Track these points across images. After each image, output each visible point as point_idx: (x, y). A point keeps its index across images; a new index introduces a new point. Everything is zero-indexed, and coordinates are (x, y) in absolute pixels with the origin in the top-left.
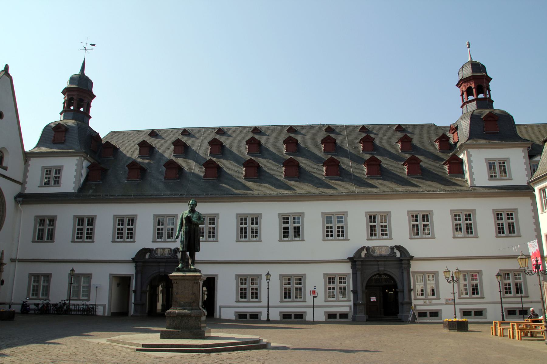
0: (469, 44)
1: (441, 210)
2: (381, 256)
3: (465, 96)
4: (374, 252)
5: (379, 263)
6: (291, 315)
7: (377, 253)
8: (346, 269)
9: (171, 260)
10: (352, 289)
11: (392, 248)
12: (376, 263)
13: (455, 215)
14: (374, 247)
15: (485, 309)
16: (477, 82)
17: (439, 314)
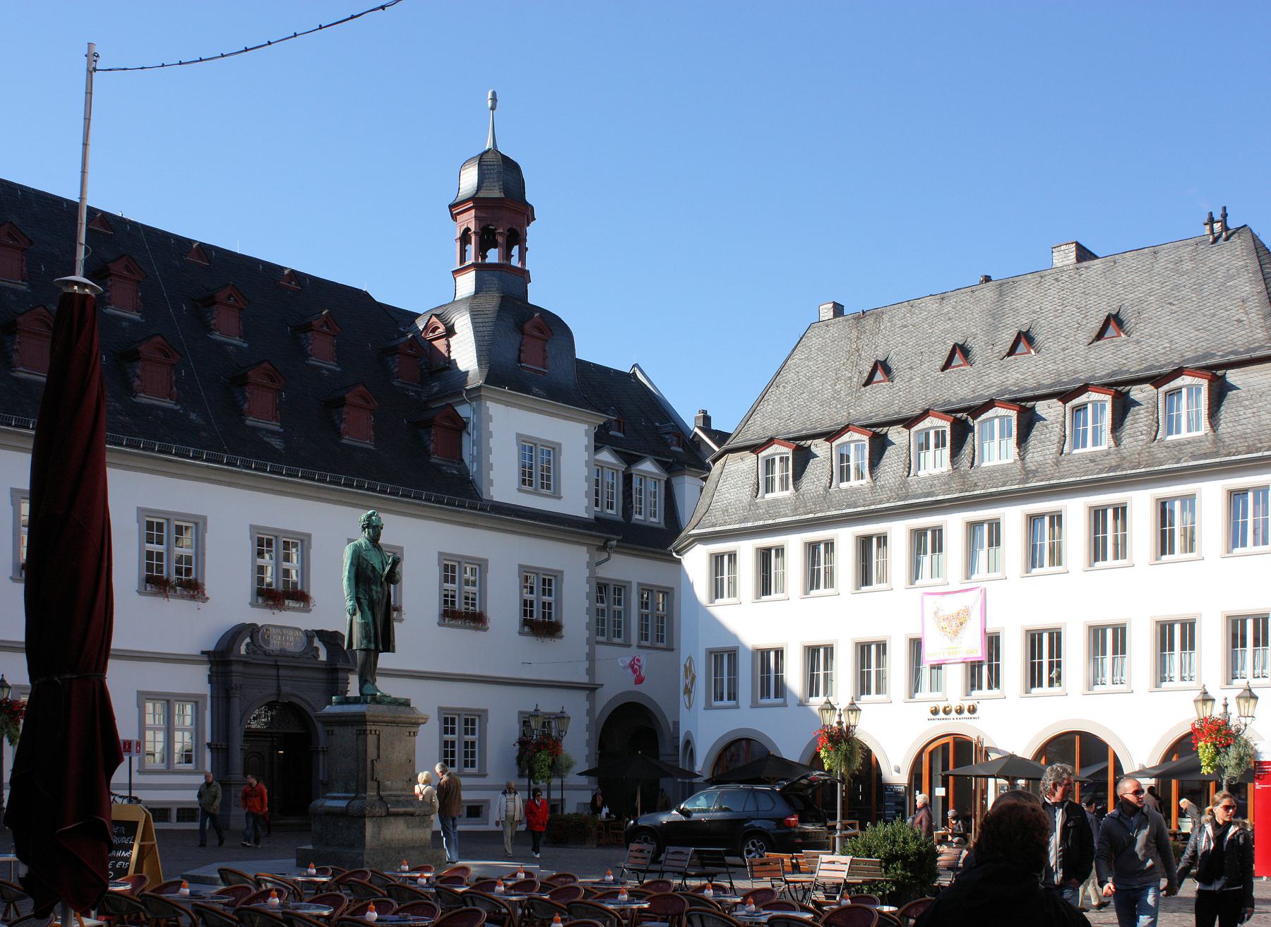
0: (494, 99)
1: (422, 542)
2: (283, 654)
3: (471, 249)
4: (267, 642)
5: (282, 672)
6: (168, 810)
7: (275, 644)
8: (197, 680)
9: (334, 659)
10: (208, 739)
11: (310, 635)
12: (274, 672)
13: (150, 525)
14: (267, 627)
15: (487, 801)
16: (500, 213)
17: (484, 810)
